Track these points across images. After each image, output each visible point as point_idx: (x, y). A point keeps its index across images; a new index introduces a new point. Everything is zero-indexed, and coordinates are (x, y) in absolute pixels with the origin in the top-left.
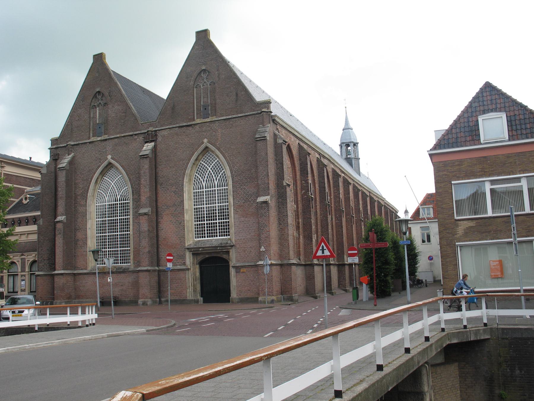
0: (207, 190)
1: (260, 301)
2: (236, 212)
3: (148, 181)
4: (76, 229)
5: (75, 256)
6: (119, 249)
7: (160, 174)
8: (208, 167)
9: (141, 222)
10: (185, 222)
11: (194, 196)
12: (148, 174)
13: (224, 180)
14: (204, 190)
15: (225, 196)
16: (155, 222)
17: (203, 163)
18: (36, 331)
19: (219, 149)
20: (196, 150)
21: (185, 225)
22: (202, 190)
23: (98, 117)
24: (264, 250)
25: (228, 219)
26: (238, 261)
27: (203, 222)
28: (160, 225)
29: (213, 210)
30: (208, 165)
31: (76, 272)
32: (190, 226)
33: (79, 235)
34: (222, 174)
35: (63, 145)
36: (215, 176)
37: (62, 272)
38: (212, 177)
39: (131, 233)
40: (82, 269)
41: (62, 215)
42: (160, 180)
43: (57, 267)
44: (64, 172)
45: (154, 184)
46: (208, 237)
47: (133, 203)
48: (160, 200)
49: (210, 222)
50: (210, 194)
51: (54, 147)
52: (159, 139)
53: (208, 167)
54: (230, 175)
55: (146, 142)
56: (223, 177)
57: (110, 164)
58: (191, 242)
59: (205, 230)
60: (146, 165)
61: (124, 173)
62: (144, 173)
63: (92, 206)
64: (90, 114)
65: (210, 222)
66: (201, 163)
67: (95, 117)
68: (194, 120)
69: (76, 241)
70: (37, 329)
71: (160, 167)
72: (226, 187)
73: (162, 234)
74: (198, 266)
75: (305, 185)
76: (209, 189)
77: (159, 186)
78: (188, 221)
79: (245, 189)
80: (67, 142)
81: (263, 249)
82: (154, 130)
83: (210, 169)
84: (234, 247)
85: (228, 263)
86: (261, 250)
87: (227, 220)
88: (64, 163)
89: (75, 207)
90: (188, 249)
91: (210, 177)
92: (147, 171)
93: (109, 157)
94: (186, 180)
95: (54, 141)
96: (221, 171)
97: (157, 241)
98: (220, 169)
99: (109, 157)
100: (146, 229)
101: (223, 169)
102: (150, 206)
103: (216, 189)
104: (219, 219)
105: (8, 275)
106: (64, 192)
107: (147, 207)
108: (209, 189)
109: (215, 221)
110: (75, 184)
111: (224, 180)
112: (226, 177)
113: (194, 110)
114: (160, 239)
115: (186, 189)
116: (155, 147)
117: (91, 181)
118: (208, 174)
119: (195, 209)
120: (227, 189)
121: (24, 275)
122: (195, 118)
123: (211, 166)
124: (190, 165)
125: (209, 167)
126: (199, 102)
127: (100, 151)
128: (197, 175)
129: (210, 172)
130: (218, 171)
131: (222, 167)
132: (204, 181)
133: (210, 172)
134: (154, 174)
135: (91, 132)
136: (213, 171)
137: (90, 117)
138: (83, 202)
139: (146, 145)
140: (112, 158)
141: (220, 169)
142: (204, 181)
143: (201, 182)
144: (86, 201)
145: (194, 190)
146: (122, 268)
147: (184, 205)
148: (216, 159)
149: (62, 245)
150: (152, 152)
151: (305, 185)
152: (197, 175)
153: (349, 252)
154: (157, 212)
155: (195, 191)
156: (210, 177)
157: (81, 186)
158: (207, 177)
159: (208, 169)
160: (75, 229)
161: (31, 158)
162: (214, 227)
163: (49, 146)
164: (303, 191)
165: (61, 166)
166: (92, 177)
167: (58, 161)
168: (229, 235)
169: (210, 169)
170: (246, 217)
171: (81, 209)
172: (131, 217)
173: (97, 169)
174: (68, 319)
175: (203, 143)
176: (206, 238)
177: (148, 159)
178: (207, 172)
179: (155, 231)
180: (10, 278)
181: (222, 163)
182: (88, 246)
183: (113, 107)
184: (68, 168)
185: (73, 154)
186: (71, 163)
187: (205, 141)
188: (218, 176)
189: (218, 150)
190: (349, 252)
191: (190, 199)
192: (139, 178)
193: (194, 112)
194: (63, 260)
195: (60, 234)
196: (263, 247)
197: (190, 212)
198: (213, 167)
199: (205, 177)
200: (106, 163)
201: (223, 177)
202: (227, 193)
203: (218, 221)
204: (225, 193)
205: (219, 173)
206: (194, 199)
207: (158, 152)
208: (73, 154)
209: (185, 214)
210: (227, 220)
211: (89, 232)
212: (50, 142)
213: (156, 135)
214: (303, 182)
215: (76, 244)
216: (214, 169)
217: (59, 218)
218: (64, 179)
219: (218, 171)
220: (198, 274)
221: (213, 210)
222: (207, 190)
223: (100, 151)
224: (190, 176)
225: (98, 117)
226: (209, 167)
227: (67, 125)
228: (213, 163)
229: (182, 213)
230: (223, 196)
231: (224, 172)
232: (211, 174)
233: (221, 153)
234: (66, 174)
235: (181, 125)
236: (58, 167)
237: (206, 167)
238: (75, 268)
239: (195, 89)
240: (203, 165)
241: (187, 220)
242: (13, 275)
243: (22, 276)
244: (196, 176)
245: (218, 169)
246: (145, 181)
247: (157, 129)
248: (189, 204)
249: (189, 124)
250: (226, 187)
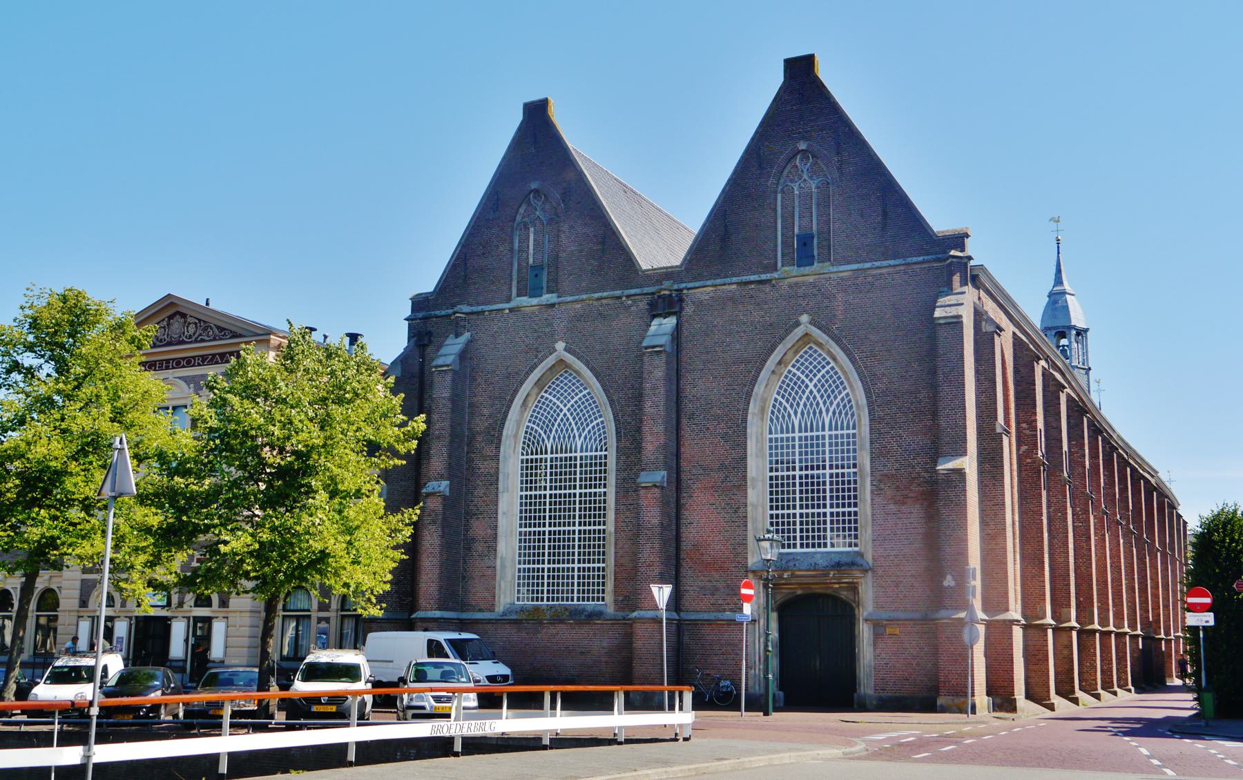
0: (834, 433)
1: (941, 706)
2: (877, 491)
3: (661, 408)
4: (469, 515)
5: (464, 578)
6: (576, 565)
7: (689, 391)
8: (807, 381)
9: (643, 502)
10: (749, 509)
11: (771, 448)
12: (662, 390)
13: (846, 414)
14: (797, 435)
15: (848, 451)
16: (673, 505)
17: (794, 370)
18: (545, 748)
19: (838, 341)
20: (782, 339)
21: (749, 515)
22: (790, 435)
23: (531, 251)
24: (952, 584)
25: (856, 505)
26: (878, 606)
27: (791, 511)
28: (686, 513)
29: (818, 484)
30: (807, 376)
31: (465, 616)
32: (760, 518)
33: (478, 528)
34: (842, 399)
35: (443, 313)
36: (825, 403)
37: (438, 614)
38: (818, 404)
39: (610, 527)
40: (480, 610)
41: (442, 477)
42: (688, 407)
43: (422, 602)
44: (449, 378)
45: (674, 416)
46: (833, 545)
47: (618, 458)
48: (686, 451)
49: (841, 510)
50: (812, 446)
51: (420, 315)
52: (689, 310)
53: (807, 381)
54: (865, 401)
55: (654, 317)
56: (845, 406)
57: (561, 361)
58: (755, 560)
59: (795, 531)
60: (657, 372)
61: (596, 385)
62: (654, 388)
63: (511, 461)
64: (512, 243)
65: (786, 512)
66: (789, 372)
67: (523, 250)
68: (776, 270)
69: (469, 543)
70: (458, 747)
71: (688, 378)
72: (851, 432)
73: (690, 534)
74: (774, 616)
75: (1027, 432)
76: (809, 434)
77: (684, 421)
78: (755, 507)
79: (901, 437)
80: (453, 306)
81: (949, 581)
82: (676, 287)
83: (811, 386)
84: (870, 573)
85: (853, 609)
86: (946, 583)
87: (852, 509)
88: (450, 350)
89: (470, 461)
90: (754, 572)
91: (811, 405)
92: (661, 384)
93: (560, 346)
94: (753, 408)
95: (420, 303)
96: (840, 393)
97: (678, 548)
98: (837, 387)
99: (560, 346)
100: (655, 521)
101: (845, 388)
102: (667, 467)
103: (797, 435)
104: (832, 506)
105: (343, 616)
106: (447, 424)
107: (657, 469)
108: (809, 434)
109: (791, 511)
110: (471, 405)
111: (846, 414)
112: (851, 407)
113: (776, 246)
114: (686, 546)
115: (752, 430)
116: (678, 327)
117: (511, 401)
118: (808, 398)
119: (771, 478)
120: (854, 435)
121: (327, 620)
122: (779, 264)
123: (815, 380)
124: (764, 374)
125: (811, 380)
126: (788, 226)
127: (536, 331)
128: (779, 398)
129: (811, 392)
130: (833, 391)
131: (842, 383)
132: (796, 413)
133: (811, 392)
134: (674, 392)
135: (514, 283)
136: (819, 391)
137: (512, 250)
138: (489, 451)
139: (656, 322)
140: (567, 350)
141: (837, 387)
142: (796, 413)
143: (789, 415)
144: (498, 448)
145: (771, 433)
146: (584, 610)
147: (746, 468)
148: (828, 363)
149: (437, 550)
150: (672, 341)
151: (1027, 432)
152: (779, 398)
153: (1191, 600)
154: (677, 483)
155: (773, 436)
156: (811, 405)
157: (486, 412)
158: (805, 405)
159: (807, 386)
160: (467, 513)
161: (326, 337)
162: (789, 523)
163: (408, 312)
164: (1024, 448)
165: (440, 361)
166: (516, 392)
167: (429, 350)
168: (856, 545)
169: (811, 386)
170: (904, 503)
171: (484, 467)
172: (611, 491)
173: (528, 374)
174: (618, 720)
175: (798, 324)
176: (798, 550)
177: (663, 356)
178: (804, 392)
179: (674, 527)
180: (287, 622)
181: (845, 373)
182: (499, 555)
183: (572, 227)
184: (457, 367)
185: (467, 335)
186: (463, 355)
187: (804, 318)
188: (831, 403)
189: (837, 342)
190: (1191, 600)
191: (760, 454)
192: (638, 399)
193: (776, 251)
194: (441, 587)
195: (434, 522)
196: (949, 577)
197: (760, 485)
198: (819, 381)
199: (798, 404)
200: (550, 361)
201: (845, 406)
202: (854, 443)
203: (828, 510)
204: (848, 444)
205: (835, 397)
206: (771, 455)
207: (683, 339)
208: (467, 335)
209: (750, 491)
210: (852, 509)
211: (502, 522)
212: (410, 303)
213: (681, 300)
214: (1024, 425)
215: (469, 549)
216: (823, 386)
217: (432, 486)
218: (446, 394)
219: (833, 391)
220: (774, 634)
221: (818, 484)
222: (834, 433)
223: (536, 331)
224: (764, 400)
225: (531, 251)
226: (811, 380)
227: (454, 265)
228: (819, 371)
229: (742, 486)
230: (843, 452)
231: (847, 395)
232: (815, 398)
233: (842, 349)
234: (453, 380)
235: (744, 278)
236: (434, 363)
237: (803, 382)
238: (463, 606)
239: (779, 196)
240: (799, 378)
241: (753, 505)
242: (298, 618)
243: (320, 620)
244: (776, 400)
245: (831, 387)
246: (655, 405)
247: (683, 285)
248: (757, 467)
249: (764, 277)
250: (851, 432)
